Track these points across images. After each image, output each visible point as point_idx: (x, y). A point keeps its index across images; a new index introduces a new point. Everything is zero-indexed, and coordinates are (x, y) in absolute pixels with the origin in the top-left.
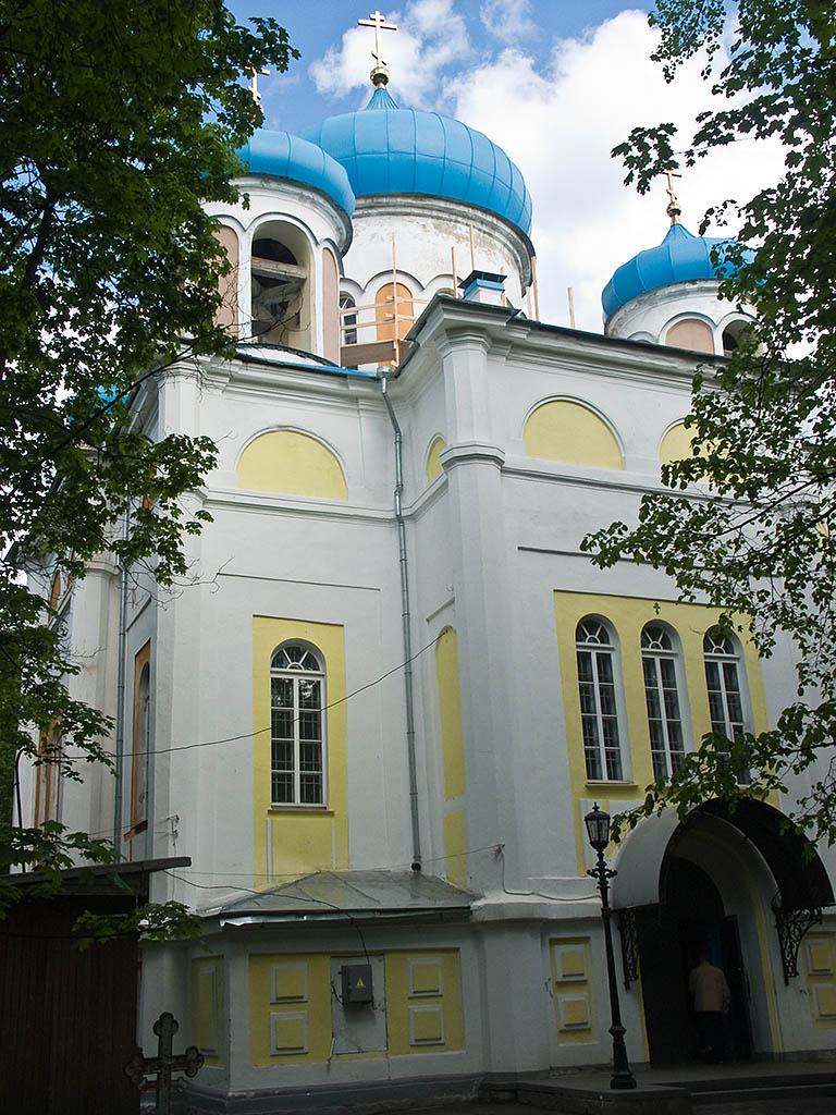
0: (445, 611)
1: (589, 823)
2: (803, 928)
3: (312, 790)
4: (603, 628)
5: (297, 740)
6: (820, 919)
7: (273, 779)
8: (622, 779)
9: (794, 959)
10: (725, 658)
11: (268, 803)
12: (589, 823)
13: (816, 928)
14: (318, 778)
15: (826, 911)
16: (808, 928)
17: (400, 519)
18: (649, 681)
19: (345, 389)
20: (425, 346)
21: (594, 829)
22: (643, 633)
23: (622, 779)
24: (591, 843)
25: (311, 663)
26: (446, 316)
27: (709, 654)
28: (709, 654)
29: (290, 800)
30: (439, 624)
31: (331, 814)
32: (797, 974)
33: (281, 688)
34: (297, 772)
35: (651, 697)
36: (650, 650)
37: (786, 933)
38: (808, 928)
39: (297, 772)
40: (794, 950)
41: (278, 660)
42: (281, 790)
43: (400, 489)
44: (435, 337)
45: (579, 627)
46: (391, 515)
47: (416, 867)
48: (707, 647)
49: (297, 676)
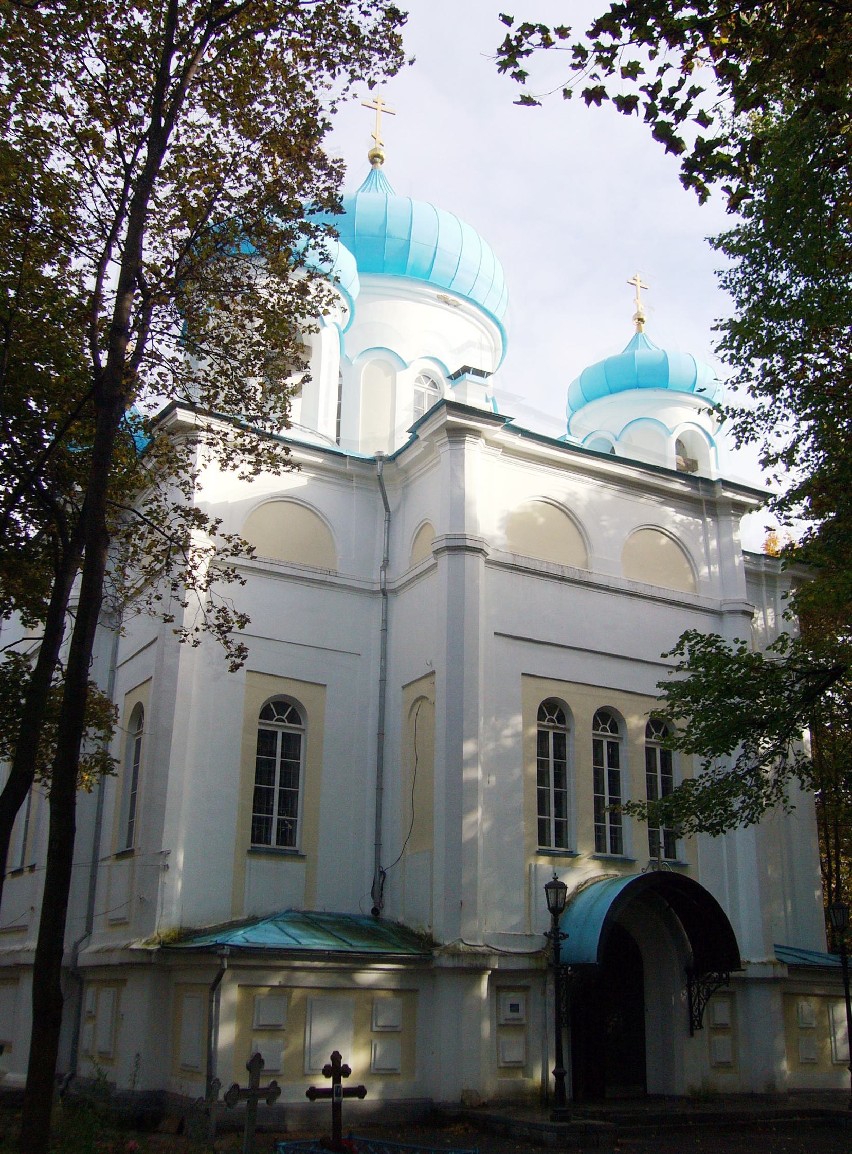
0: (423, 681)
1: (549, 890)
2: (712, 989)
3: (287, 836)
4: (560, 710)
5: (277, 788)
6: (727, 981)
7: (254, 822)
8: (567, 847)
9: (701, 1014)
10: (610, 737)
11: (249, 844)
12: (549, 890)
13: (723, 988)
14: (293, 823)
15: (733, 974)
16: (716, 988)
17: (384, 592)
18: (598, 760)
19: (343, 467)
20: (425, 440)
21: (552, 896)
22: (595, 717)
23: (567, 847)
24: (549, 908)
25: (295, 718)
26: (450, 418)
27: (597, 732)
28: (597, 732)
29: (268, 842)
30: (414, 693)
31: (303, 857)
32: (702, 1027)
33: (265, 740)
34: (275, 817)
35: (598, 773)
36: (545, 723)
37: (696, 991)
38: (716, 988)
39: (275, 817)
40: (701, 1007)
41: (266, 713)
42: (259, 832)
43: (386, 564)
44: (435, 433)
45: (540, 709)
46: (377, 587)
47: (376, 911)
48: (596, 726)
49: (280, 727)
